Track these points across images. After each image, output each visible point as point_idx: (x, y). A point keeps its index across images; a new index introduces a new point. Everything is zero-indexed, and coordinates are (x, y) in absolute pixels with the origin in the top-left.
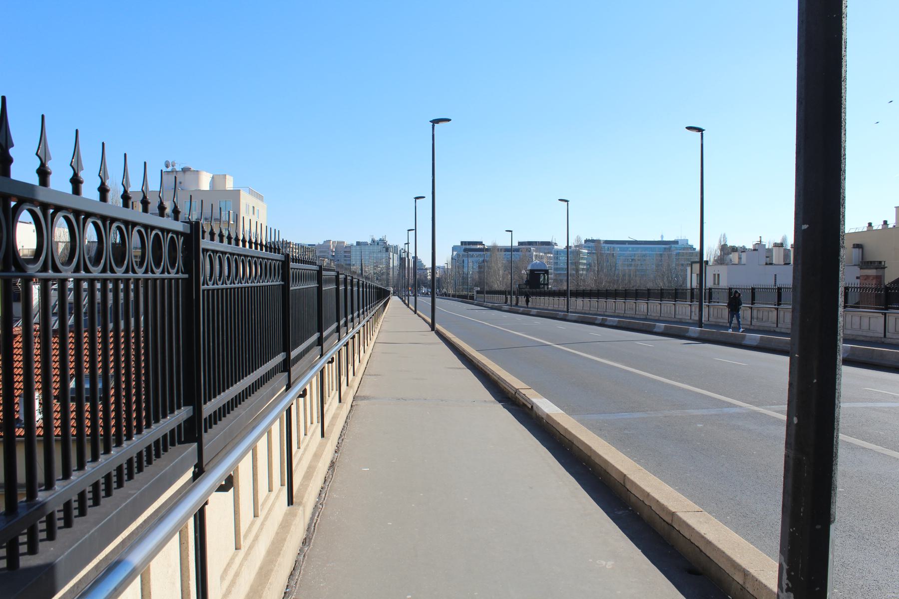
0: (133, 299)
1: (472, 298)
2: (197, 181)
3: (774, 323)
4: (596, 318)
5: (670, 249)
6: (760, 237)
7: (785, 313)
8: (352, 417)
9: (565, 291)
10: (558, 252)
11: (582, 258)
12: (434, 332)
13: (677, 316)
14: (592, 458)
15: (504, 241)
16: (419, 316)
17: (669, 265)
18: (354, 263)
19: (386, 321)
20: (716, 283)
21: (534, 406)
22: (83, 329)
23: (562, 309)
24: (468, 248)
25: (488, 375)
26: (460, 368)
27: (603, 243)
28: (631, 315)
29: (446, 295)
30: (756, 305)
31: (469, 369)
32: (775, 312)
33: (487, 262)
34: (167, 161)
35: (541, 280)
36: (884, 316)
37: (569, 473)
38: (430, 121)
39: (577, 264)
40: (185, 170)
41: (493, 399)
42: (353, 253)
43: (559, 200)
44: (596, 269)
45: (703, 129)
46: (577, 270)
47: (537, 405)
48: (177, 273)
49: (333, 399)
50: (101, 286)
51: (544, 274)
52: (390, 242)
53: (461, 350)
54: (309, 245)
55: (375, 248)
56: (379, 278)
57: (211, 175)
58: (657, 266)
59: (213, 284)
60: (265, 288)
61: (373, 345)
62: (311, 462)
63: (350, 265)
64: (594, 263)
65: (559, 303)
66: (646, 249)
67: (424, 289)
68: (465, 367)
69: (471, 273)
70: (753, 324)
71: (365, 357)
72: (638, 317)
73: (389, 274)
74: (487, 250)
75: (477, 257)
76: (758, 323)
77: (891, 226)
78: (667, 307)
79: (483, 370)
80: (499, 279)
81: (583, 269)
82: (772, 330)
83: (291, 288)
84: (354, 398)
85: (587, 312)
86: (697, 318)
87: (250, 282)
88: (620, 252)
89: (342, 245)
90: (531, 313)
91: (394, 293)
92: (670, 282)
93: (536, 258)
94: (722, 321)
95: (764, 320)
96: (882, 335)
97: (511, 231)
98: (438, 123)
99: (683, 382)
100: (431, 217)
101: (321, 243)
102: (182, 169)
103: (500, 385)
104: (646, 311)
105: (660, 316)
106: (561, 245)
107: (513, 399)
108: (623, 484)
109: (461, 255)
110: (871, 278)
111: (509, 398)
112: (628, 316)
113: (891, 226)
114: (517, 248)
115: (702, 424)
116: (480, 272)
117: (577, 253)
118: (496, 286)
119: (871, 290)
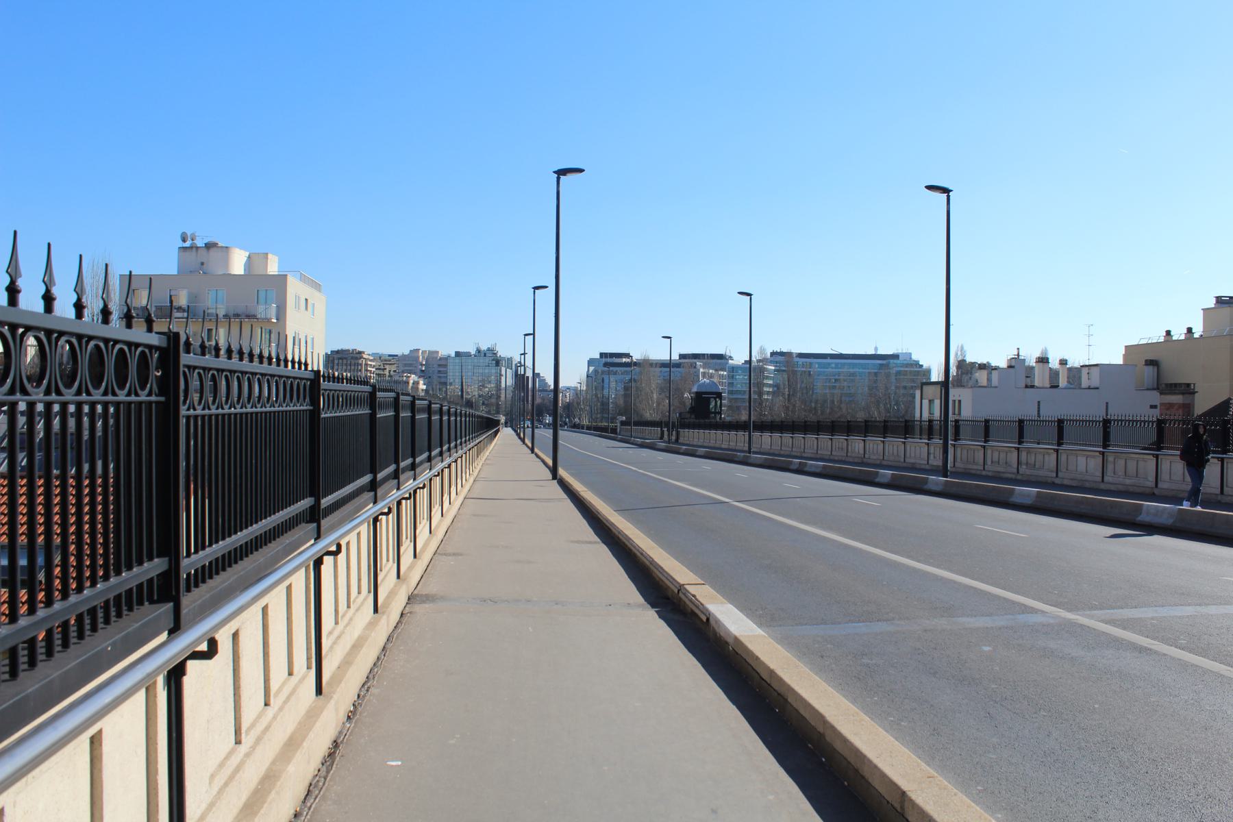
0: (113, 429)
1: (614, 431)
2: (226, 261)
3: (1052, 471)
4: (791, 462)
5: (887, 365)
6: (1018, 349)
7: (1069, 457)
8: (397, 638)
9: (745, 422)
10: (734, 369)
11: (767, 378)
12: (556, 481)
13: (907, 460)
14: (828, 739)
15: (660, 353)
16: (537, 456)
17: (887, 388)
18: (452, 381)
19: (487, 464)
20: (957, 412)
21: (711, 619)
22: (37, 473)
23: (741, 448)
24: (610, 363)
25: (635, 555)
26: (590, 543)
27: (796, 357)
28: (840, 458)
29: (576, 427)
30: (1025, 445)
31: (605, 544)
32: (1054, 455)
33: (635, 381)
34: (183, 233)
35: (711, 406)
36: (1220, 462)
37: (785, 770)
38: (554, 172)
39: (760, 385)
40: (210, 246)
41: (641, 600)
42: (450, 367)
43: (739, 293)
44: (787, 393)
45: (950, 188)
46: (760, 394)
47: (716, 617)
48: (150, 394)
49: (357, 610)
50: (90, 409)
51: (715, 398)
52: (502, 352)
53: (594, 511)
54: (390, 356)
55: (481, 361)
56: (486, 402)
57: (247, 254)
58: (871, 388)
59: (242, 408)
60: (286, 414)
61: (461, 502)
62: (274, 763)
63: (445, 384)
64: (784, 385)
65: (737, 440)
66: (854, 365)
67: (548, 418)
68: (599, 540)
69: (613, 396)
70: (1020, 472)
71: (441, 524)
72: (851, 460)
73: (500, 397)
74: (635, 364)
75: (622, 374)
76: (1027, 470)
77: (1196, 335)
78: (894, 447)
79: (627, 546)
80: (653, 405)
81: (768, 393)
82: (1049, 480)
83: (323, 416)
84: (409, 599)
85: (777, 452)
86: (939, 463)
87: (276, 405)
88: (819, 370)
89: (435, 356)
90: (697, 454)
91: (506, 423)
92: (888, 411)
93: (704, 376)
94: (975, 467)
95: (1036, 467)
96: (1218, 491)
97: (670, 338)
98: (565, 175)
99: (938, 567)
100: (554, 312)
101: (407, 352)
102: (206, 244)
103: (653, 574)
104: (862, 452)
105: (847, 456)
106: (739, 357)
107: (675, 601)
108: (899, 809)
109: (600, 371)
110: (1176, 407)
111: (668, 599)
112: (836, 458)
113: (1196, 335)
114: (678, 362)
115: (989, 646)
116: (625, 396)
117: (762, 370)
118: (649, 415)
119: (1177, 423)
